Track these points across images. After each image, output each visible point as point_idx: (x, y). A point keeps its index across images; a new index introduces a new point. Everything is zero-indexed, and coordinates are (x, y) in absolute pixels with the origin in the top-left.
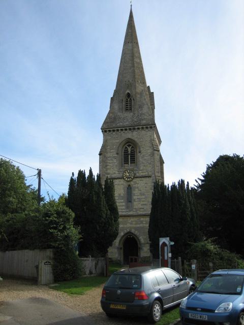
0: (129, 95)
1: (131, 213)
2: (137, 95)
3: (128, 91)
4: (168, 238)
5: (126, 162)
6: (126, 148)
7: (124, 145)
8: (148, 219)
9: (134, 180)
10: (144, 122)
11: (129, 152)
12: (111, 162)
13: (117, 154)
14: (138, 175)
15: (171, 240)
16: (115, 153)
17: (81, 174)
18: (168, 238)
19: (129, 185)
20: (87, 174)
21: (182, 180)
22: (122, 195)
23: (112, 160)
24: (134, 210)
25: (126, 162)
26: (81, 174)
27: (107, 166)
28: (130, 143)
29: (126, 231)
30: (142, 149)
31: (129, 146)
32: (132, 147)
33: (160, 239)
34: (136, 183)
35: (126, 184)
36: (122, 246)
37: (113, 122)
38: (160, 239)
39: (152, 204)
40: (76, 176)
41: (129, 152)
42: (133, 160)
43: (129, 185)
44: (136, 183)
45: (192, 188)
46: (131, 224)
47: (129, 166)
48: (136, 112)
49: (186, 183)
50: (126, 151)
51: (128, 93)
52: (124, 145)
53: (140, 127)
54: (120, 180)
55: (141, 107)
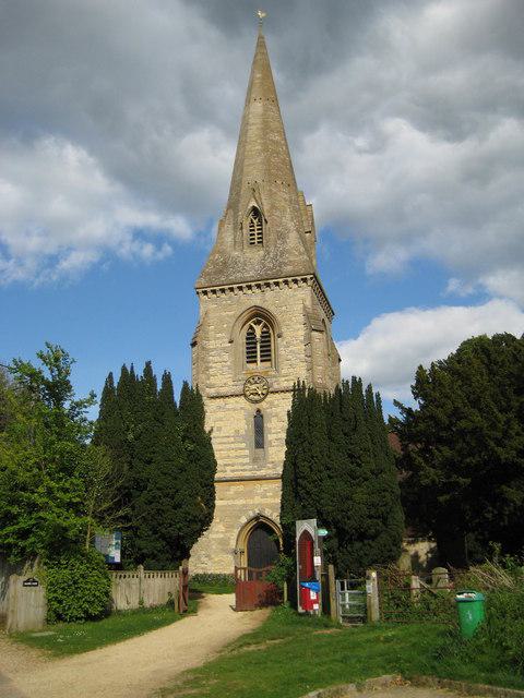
0: (256, 212)
1: (262, 473)
2: (449, 412)
3: (253, 203)
4: (314, 522)
5: (251, 358)
6: (251, 327)
7: (249, 320)
8: (278, 485)
9: (268, 399)
10: (289, 268)
11: (258, 336)
12: (216, 359)
13: (231, 342)
14: (276, 386)
15: (322, 524)
16: (227, 340)
17: (127, 376)
18: (314, 522)
19: (258, 411)
20: (139, 372)
21: (354, 378)
22: (242, 432)
23: (219, 355)
24: (270, 465)
25: (251, 358)
26: (127, 376)
27: (207, 369)
28: (260, 315)
29: (252, 514)
30: (284, 329)
31: (258, 323)
32: (265, 326)
33: (298, 523)
34: (272, 404)
35: (252, 408)
36: (243, 546)
37: (221, 272)
38: (298, 523)
39: (288, 443)
40: (116, 380)
41: (258, 336)
42: (266, 357)
43: (258, 411)
44: (272, 404)
45: (390, 419)
46: (264, 496)
47: (260, 366)
48: (272, 249)
49: (364, 388)
50: (251, 336)
51: (254, 209)
52: (247, 322)
53: (281, 280)
54: (237, 399)
55: (282, 236)
